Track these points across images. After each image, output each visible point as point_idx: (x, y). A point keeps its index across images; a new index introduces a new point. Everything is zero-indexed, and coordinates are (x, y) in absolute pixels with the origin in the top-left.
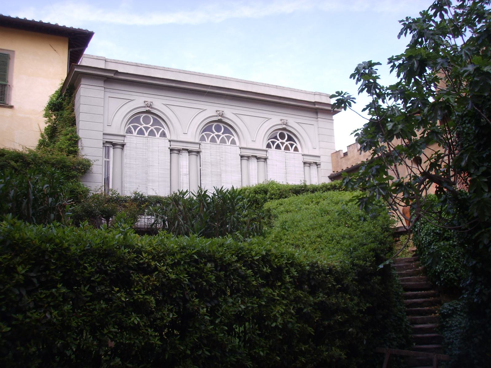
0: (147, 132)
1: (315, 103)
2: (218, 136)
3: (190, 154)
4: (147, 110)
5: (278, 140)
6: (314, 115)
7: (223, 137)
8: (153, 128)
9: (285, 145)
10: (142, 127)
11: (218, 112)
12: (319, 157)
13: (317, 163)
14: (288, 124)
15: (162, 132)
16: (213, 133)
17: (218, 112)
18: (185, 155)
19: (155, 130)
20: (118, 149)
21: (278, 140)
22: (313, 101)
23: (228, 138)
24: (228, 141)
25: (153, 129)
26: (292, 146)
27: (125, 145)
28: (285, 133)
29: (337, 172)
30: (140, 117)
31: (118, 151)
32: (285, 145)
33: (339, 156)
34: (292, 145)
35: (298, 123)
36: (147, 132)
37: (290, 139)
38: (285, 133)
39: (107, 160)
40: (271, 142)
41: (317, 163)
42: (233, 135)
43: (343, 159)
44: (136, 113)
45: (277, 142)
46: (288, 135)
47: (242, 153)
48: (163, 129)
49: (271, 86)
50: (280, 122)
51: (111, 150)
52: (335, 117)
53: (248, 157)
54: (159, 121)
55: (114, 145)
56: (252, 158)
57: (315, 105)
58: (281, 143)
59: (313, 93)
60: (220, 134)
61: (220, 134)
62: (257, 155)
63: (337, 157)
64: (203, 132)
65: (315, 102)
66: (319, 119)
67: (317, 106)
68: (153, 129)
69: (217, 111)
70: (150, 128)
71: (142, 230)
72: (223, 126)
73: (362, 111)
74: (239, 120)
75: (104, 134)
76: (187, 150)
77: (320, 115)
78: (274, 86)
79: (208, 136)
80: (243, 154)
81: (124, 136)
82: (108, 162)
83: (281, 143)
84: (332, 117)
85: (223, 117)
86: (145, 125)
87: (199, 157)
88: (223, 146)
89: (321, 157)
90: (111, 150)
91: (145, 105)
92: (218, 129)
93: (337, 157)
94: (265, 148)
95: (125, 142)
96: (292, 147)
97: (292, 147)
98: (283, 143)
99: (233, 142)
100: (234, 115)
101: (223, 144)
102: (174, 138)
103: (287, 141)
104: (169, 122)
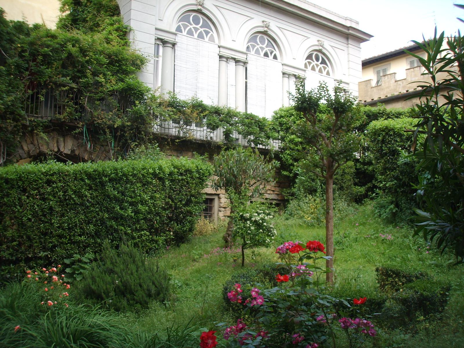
0: (196, 33)
1: (349, 28)
2: (196, 29)
3: (237, 64)
4: (198, 9)
5: (314, 62)
6: (344, 41)
7: (191, 28)
8: (202, 30)
9: (319, 67)
10: (191, 27)
11: (265, 23)
12: (348, 84)
13: (346, 91)
14: (205, 6)
15: (200, 33)
16: (191, 25)
17: (265, 23)
18: (232, 64)
19: (204, 33)
20: (169, 48)
21: (258, 45)
22: (348, 26)
23: (207, 33)
24: (253, 50)
25: (203, 31)
26: (271, 53)
27: (176, 44)
28: (320, 55)
29: (365, 101)
30: (190, 16)
31: (169, 50)
32: (319, 67)
33: (369, 85)
34: (325, 68)
35: (332, 46)
36: (196, 33)
37: (323, 62)
38: (320, 55)
39: (157, 59)
40: (308, 62)
41: (346, 91)
42: (327, 65)
43: (375, 89)
44: (188, 10)
45: (257, 47)
46: (322, 58)
47: (221, 53)
48: (211, 33)
49: (310, 4)
50: (261, 24)
51: (161, 48)
52: (363, 45)
53: (227, 58)
54: (208, 24)
55: (164, 42)
56: (231, 60)
57: (348, 30)
58: (316, 64)
59: (345, 18)
60: (198, 27)
61: (198, 27)
62: (236, 57)
63: (366, 86)
64: (179, 22)
65: (351, 27)
66: (350, 46)
67: (351, 32)
68: (203, 31)
69: (263, 22)
70: (199, 29)
71: (197, 142)
72: (267, 39)
73: (372, 36)
74: (281, 33)
75: (156, 29)
76: (234, 59)
77: (350, 42)
78: (313, 4)
79: (185, 27)
80: (222, 54)
81: (176, 34)
82: (157, 61)
83: (316, 64)
84: (360, 45)
85: (203, 7)
86: (261, 46)
87: (174, 49)
88: (200, 42)
89: (350, 84)
90: (161, 48)
91: (263, 25)
92: (196, 21)
93: (366, 86)
94: (244, 50)
95: (176, 41)
96: (207, 36)
97: (207, 36)
98: (317, 65)
99: (212, 39)
100: (278, 29)
101: (200, 39)
102: (222, 44)
103: (201, 27)
104: (219, 25)
